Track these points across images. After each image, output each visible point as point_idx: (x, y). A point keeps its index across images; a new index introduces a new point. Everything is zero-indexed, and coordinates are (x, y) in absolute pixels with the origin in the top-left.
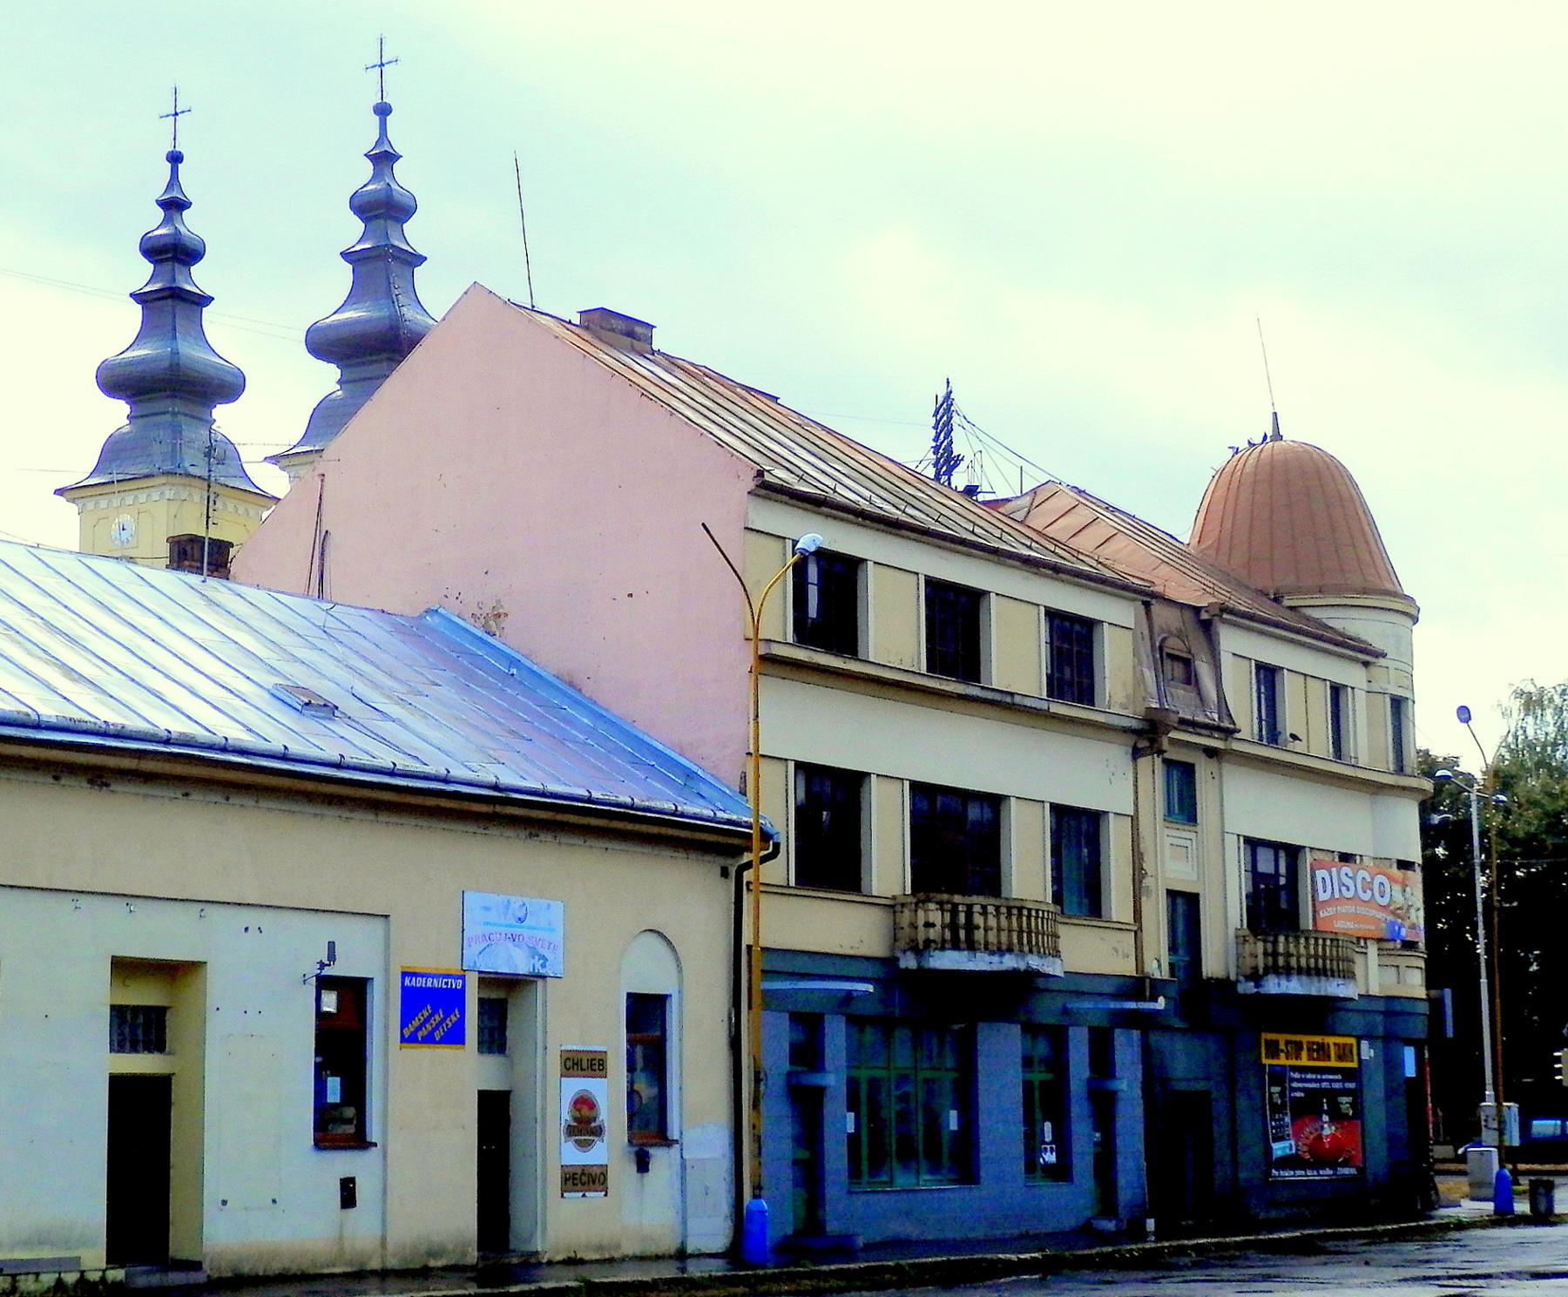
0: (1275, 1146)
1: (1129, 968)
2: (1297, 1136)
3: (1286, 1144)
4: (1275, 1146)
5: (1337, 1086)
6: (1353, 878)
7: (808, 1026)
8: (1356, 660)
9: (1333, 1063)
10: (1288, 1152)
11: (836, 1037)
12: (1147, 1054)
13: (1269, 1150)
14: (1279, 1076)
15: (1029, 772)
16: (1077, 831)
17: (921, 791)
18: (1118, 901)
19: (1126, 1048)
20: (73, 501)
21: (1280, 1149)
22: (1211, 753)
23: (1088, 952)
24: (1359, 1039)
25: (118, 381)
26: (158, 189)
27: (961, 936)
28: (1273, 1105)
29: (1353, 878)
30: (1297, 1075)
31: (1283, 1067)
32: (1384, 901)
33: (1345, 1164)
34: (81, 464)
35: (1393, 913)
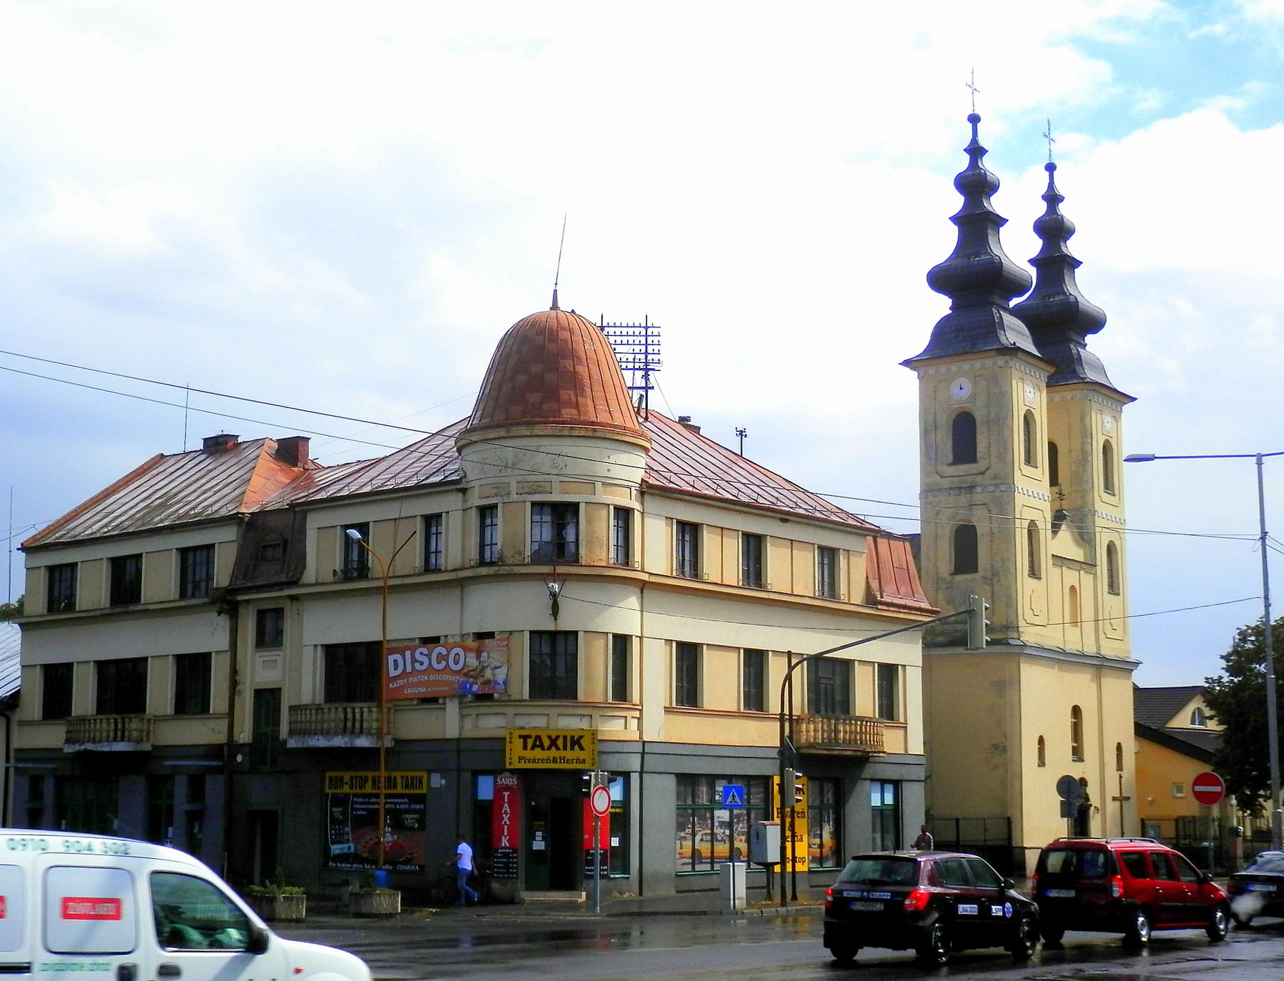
0: (333, 847)
1: (221, 738)
2: (356, 841)
3: (346, 846)
4: (333, 847)
5: (402, 807)
6: (429, 656)
7: (36, 782)
8: (451, 491)
9: (399, 790)
10: (346, 851)
11: (49, 787)
12: (230, 786)
13: (327, 850)
14: (340, 801)
15: (156, 643)
16: (193, 670)
17: (101, 665)
18: (218, 700)
19: (215, 789)
20: (914, 369)
21: (336, 849)
22: (294, 598)
23: (198, 733)
24: (429, 772)
25: (940, 279)
26: (966, 142)
27: (120, 735)
28: (335, 821)
29: (429, 656)
30: (361, 800)
31: (347, 795)
32: (458, 667)
33: (407, 862)
34: (919, 342)
35: (466, 675)
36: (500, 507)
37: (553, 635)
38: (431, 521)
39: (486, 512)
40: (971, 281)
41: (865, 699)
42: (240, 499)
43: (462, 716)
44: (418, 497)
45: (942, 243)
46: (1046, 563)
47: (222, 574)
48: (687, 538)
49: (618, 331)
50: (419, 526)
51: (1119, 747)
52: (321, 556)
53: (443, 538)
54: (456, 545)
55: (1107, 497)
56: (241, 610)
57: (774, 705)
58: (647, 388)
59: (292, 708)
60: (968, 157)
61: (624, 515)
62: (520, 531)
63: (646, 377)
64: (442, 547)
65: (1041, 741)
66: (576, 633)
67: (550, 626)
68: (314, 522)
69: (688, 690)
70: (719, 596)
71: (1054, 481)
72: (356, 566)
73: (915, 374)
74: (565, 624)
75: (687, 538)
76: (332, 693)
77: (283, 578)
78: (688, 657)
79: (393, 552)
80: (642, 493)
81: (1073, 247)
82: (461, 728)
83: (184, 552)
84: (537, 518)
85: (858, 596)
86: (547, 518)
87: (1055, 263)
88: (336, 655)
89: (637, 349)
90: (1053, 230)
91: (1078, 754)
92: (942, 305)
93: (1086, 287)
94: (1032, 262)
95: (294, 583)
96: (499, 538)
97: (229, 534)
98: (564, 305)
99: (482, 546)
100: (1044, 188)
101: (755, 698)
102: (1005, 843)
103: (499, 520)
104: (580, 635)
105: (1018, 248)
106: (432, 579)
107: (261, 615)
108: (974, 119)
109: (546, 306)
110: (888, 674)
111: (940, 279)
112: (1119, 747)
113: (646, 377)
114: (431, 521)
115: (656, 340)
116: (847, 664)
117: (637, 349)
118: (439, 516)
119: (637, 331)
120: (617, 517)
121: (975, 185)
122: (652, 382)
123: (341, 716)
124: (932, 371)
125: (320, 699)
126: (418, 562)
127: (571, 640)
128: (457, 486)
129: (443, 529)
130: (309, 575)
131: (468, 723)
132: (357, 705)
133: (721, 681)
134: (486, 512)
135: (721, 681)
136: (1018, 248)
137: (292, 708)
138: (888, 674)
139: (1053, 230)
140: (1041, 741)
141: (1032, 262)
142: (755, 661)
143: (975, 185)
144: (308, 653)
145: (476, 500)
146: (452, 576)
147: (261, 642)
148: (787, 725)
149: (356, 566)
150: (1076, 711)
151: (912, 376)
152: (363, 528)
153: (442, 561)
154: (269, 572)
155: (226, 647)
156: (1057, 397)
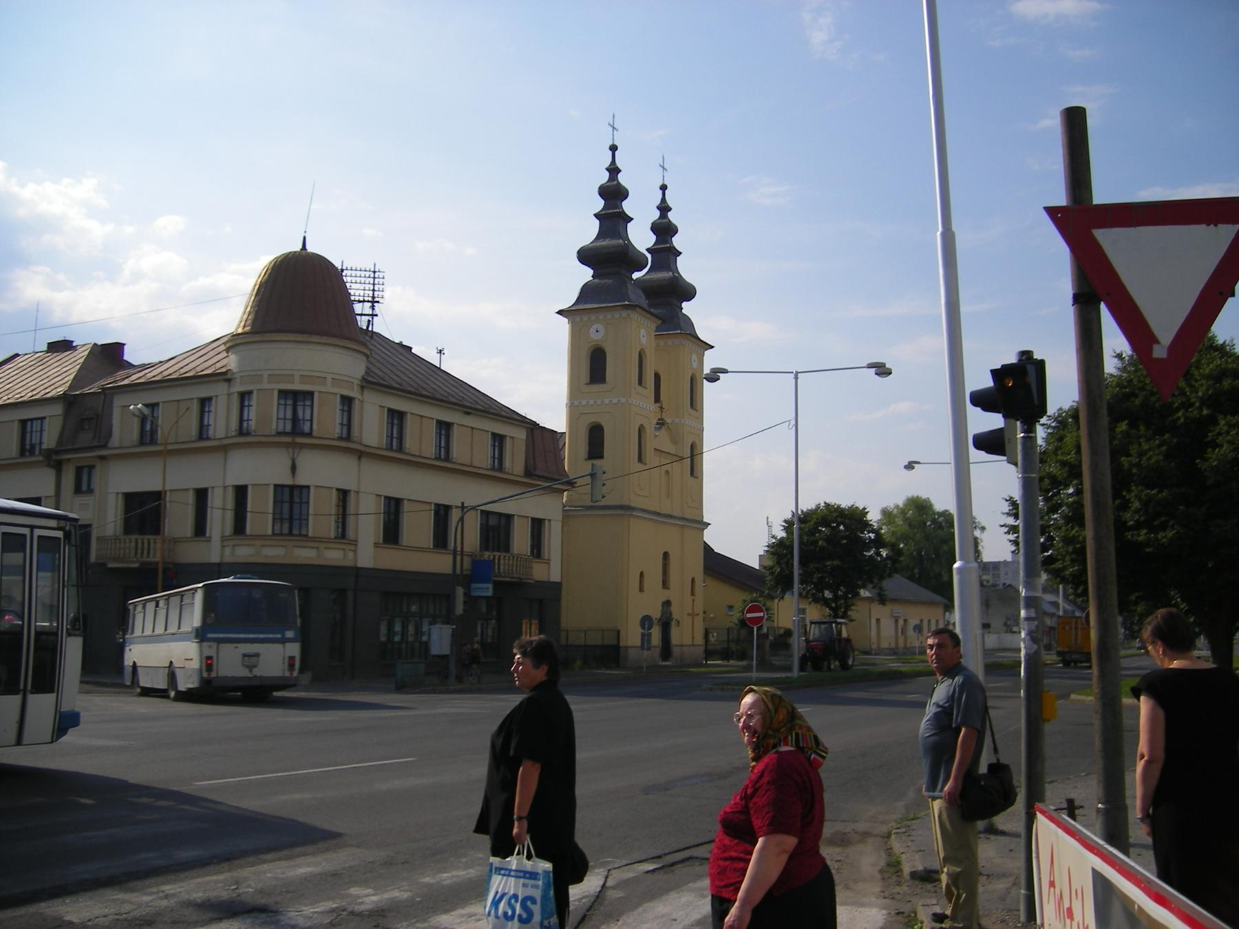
22: (102, 458)
25: (585, 256)
36: (255, 394)
37: (292, 488)
38: (204, 402)
39: (244, 396)
40: (608, 258)
41: (521, 540)
42: (1144, 846)
43: (223, 547)
44: (191, 385)
45: (589, 231)
46: (651, 458)
47: (50, 438)
48: (396, 422)
49: (354, 273)
50: (195, 406)
51: (693, 580)
52: (123, 430)
53: (212, 415)
54: (222, 421)
55: (691, 411)
56: (64, 467)
57: (451, 545)
58: (373, 315)
59: (98, 539)
60: (607, 174)
61: (347, 401)
62: (267, 414)
63: (373, 308)
64: (211, 422)
65: (642, 574)
66: (308, 487)
67: (289, 482)
68: (118, 402)
69: (391, 534)
70: (417, 464)
71: (657, 399)
72: (148, 435)
73: (566, 320)
74: (301, 480)
75: (396, 422)
76: (128, 528)
77: (95, 443)
78: (393, 507)
79: (177, 424)
80: (362, 388)
81: (677, 241)
82: (222, 556)
83: (24, 423)
84: (282, 402)
85: (519, 468)
86: (290, 402)
87: (665, 252)
88: (131, 500)
89: (367, 287)
90: (664, 230)
91: (665, 584)
92: (586, 274)
93: (687, 268)
94: (648, 250)
95: (104, 446)
96: (253, 415)
97: (58, 410)
98: (310, 249)
99: (241, 420)
100: (658, 201)
101: (441, 540)
102: (614, 642)
103: (254, 402)
104: (312, 490)
105: (641, 237)
106: (202, 443)
107: (79, 470)
108: (613, 148)
109: (298, 248)
110: (538, 525)
111: (585, 256)
112: (693, 580)
113: (373, 308)
114: (204, 402)
115: (381, 281)
116: (509, 518)
117: (367, 287)
118: (210, 399)
119: (367, 274)
120: (343, 403)
121: (613, 193)
122: (377, 311)
123: (133, 544)
124: (578, 319)
125: (120, 530)
126: (194, 431)
127: (305, 491)
128: (224, 377)
129: (212, 408)
130: (115, 440)
131: (228, 551)
132: (146, 537)
133: (416, 528)
134: (244, 396)
135: (416, 528)
136: (641, 237)
137: (98, 539)
138: (538, 525)
139: (664, 230)
140: (642, 574)
141: (648, 250)
142: (442, 513)
143: (613, 193)
144: (112, 499)
145: (238, 387)
146: (216, 443)
147: (78, 490)
148: (459, 558)
149: (148, 435)
150: (641, 589)
151: (564, 322)
152: (153, 406)
153: (211, 432)
154: (85, 438)
155: (52, 493)
156: (662, 343)
